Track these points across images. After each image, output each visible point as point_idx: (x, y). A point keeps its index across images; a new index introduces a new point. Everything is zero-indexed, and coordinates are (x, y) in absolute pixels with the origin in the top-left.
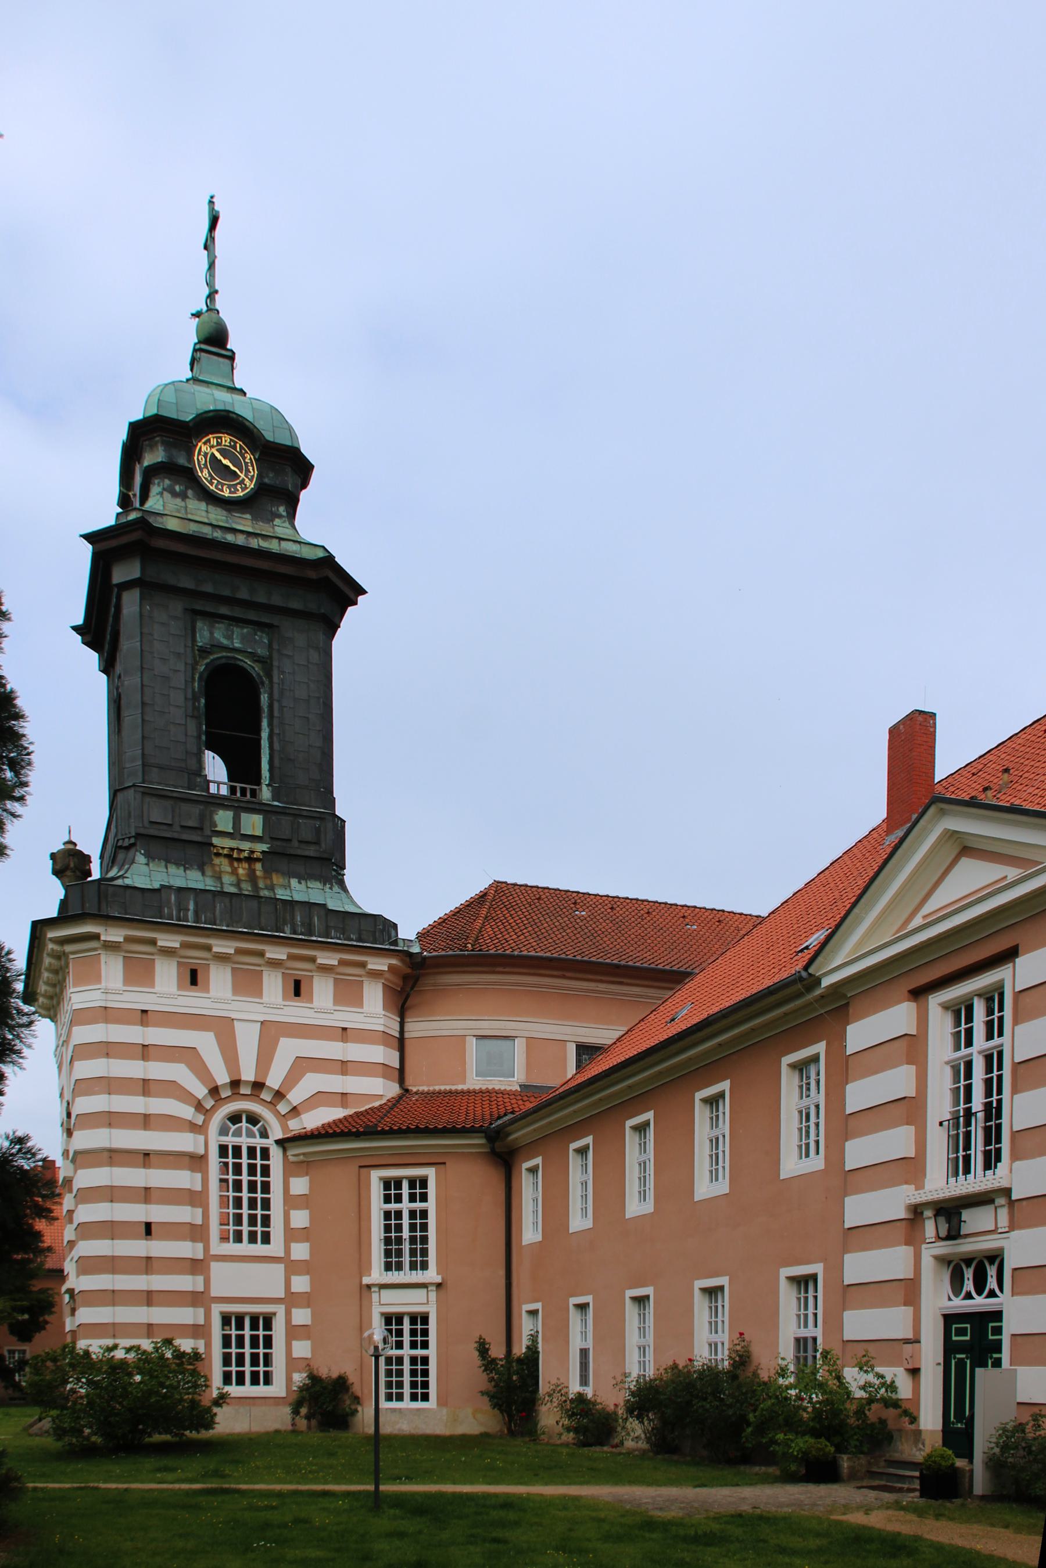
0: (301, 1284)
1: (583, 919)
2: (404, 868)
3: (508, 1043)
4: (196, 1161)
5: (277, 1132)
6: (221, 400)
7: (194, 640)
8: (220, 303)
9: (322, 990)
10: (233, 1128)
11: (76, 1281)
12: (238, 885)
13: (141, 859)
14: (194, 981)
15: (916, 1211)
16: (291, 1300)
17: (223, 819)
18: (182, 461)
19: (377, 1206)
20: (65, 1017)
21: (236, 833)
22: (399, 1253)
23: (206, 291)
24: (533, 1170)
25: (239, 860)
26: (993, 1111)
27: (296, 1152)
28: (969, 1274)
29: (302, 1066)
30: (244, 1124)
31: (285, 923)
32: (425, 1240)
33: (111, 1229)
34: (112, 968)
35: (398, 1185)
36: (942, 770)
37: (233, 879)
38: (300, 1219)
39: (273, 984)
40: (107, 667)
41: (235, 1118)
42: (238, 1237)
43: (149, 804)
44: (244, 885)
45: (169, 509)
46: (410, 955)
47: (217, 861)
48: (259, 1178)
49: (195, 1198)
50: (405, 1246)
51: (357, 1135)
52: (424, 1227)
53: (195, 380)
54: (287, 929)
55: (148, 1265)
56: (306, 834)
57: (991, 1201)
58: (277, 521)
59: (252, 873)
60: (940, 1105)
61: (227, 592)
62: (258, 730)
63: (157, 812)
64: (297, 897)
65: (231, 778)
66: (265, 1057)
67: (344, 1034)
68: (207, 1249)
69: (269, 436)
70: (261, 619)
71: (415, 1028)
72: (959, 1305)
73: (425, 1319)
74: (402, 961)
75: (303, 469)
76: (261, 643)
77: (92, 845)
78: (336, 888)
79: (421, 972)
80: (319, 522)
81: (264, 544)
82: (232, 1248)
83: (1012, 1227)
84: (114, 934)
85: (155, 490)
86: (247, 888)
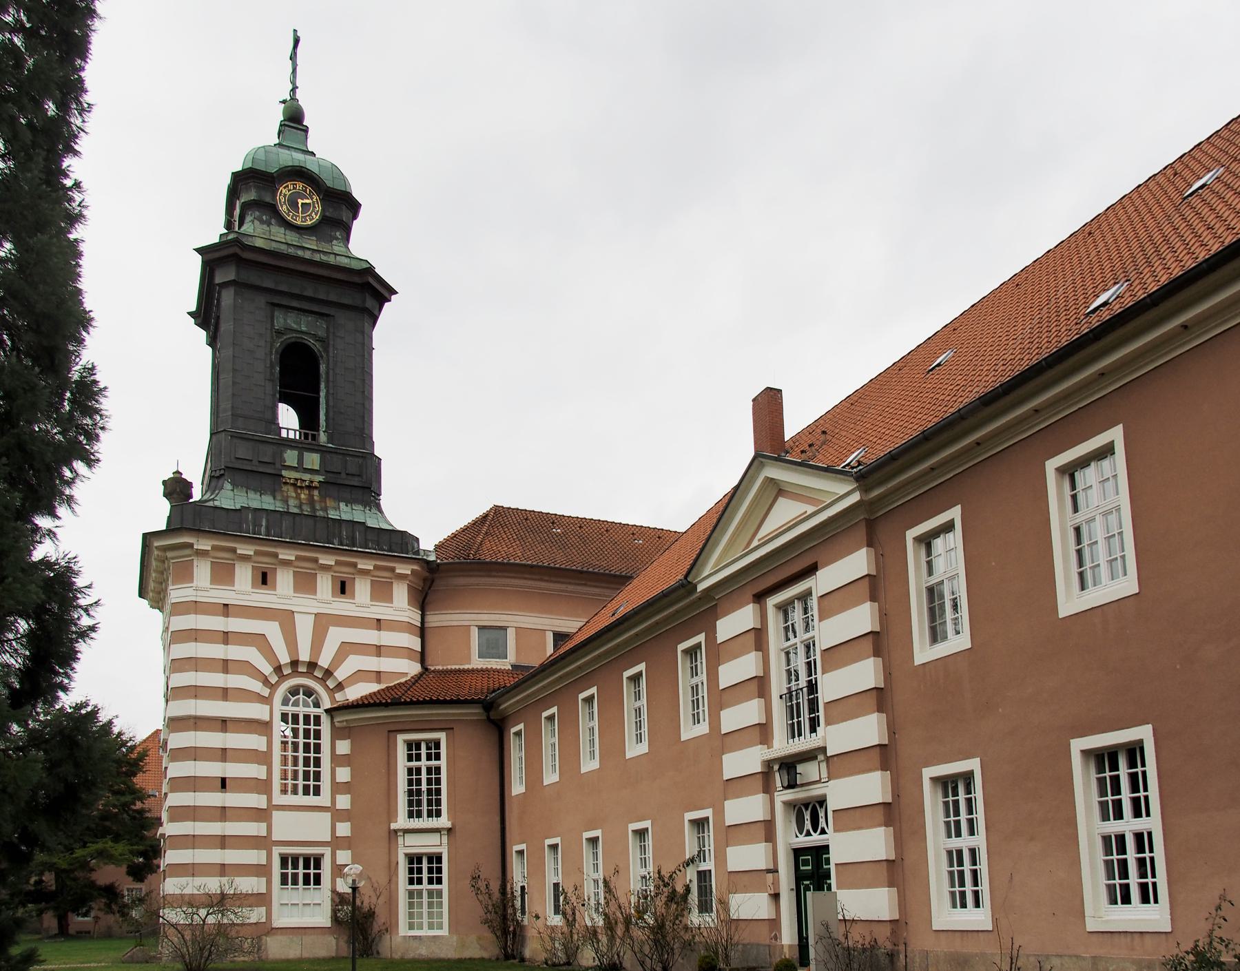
0: (344, 829)
1: (557, 535)
2: (425, 496)
3: (502, 632)
4: (264, 727)
5: (327, 704)
6: (298, 158)
7: (273, 325)
8: (299, 95)
9: (362, 588)
10: (293, 699)
11: (169, 828)
12: (300, 507)
13: (228, 486)
14: (264, 582)
15: (768, 764)
16: (336, 843)
17: (291, 457)
18: (268, 199)
19: (402, 763)
20: (168, 608)
21: (300, 468)
22: (419, 803)
23: (290, 87)
24: (518, 734)
25: (301, 487)
26: (812, 687)
27: (340, 718)
28: (807, 816)
29: (347, 649)
30: (301, 696)
31: (334, 537)
32: (438, 792)
33: (192, 784)
34: (202, 571)
35: (418, 747)
36: (789, 433)
37: (297, 502)
38: (344, 774)
39: (325, 584)
40: (212, 342)
41: (294, 691)
42: (295, 792)
43: (239, 446)
44: (305, 507)
45: (256, 231)
46: (428, 562)
47: (285, 488)
48: (312, 741)
49: (263, 758)
50: (423, 799)
51: (386, 705)
52: (438, 781)
53: (280, 145)
54: (336, 541)
55: (223, 813)
56: (352, 469)
57: (816, 758)
58: (335, 242)
59: (311, 496)
60: (778, 685)
61: (297, 291)
62: (318, 392)
63: (243, 451)
64: (344, 517)
65: (302, 426)
66: (318, 642)
67: (379, 624)
68: (270, 800)
69: (329, 184)
70: (320, 310)
71: (434, 620)
72: (803, 841)
73: (439, 859)
74: (422, 567)
75: (354, 207)
76: (321, 328)
77: (195, 474)
78: (374, 510)
79: (442, 576)
80: (366, 243)
81: (324, 258)
82: (290, 799)
83: (830, 779)
84: (204, 544)
85: (248, 218)
86: (307, 510)
